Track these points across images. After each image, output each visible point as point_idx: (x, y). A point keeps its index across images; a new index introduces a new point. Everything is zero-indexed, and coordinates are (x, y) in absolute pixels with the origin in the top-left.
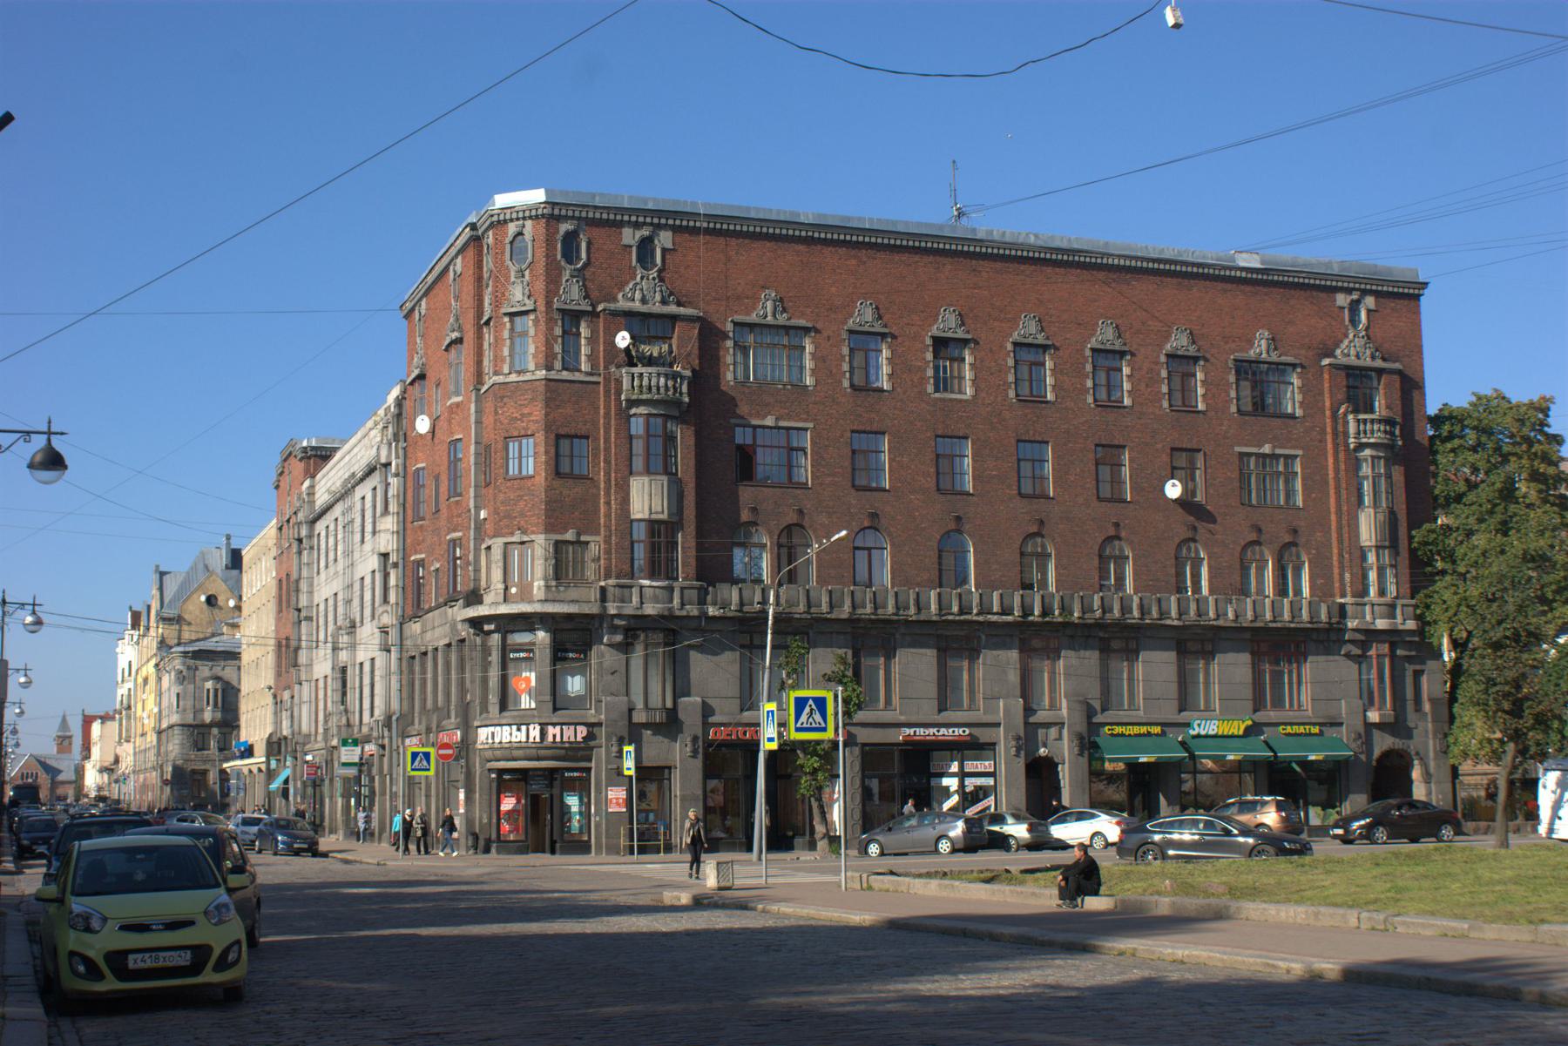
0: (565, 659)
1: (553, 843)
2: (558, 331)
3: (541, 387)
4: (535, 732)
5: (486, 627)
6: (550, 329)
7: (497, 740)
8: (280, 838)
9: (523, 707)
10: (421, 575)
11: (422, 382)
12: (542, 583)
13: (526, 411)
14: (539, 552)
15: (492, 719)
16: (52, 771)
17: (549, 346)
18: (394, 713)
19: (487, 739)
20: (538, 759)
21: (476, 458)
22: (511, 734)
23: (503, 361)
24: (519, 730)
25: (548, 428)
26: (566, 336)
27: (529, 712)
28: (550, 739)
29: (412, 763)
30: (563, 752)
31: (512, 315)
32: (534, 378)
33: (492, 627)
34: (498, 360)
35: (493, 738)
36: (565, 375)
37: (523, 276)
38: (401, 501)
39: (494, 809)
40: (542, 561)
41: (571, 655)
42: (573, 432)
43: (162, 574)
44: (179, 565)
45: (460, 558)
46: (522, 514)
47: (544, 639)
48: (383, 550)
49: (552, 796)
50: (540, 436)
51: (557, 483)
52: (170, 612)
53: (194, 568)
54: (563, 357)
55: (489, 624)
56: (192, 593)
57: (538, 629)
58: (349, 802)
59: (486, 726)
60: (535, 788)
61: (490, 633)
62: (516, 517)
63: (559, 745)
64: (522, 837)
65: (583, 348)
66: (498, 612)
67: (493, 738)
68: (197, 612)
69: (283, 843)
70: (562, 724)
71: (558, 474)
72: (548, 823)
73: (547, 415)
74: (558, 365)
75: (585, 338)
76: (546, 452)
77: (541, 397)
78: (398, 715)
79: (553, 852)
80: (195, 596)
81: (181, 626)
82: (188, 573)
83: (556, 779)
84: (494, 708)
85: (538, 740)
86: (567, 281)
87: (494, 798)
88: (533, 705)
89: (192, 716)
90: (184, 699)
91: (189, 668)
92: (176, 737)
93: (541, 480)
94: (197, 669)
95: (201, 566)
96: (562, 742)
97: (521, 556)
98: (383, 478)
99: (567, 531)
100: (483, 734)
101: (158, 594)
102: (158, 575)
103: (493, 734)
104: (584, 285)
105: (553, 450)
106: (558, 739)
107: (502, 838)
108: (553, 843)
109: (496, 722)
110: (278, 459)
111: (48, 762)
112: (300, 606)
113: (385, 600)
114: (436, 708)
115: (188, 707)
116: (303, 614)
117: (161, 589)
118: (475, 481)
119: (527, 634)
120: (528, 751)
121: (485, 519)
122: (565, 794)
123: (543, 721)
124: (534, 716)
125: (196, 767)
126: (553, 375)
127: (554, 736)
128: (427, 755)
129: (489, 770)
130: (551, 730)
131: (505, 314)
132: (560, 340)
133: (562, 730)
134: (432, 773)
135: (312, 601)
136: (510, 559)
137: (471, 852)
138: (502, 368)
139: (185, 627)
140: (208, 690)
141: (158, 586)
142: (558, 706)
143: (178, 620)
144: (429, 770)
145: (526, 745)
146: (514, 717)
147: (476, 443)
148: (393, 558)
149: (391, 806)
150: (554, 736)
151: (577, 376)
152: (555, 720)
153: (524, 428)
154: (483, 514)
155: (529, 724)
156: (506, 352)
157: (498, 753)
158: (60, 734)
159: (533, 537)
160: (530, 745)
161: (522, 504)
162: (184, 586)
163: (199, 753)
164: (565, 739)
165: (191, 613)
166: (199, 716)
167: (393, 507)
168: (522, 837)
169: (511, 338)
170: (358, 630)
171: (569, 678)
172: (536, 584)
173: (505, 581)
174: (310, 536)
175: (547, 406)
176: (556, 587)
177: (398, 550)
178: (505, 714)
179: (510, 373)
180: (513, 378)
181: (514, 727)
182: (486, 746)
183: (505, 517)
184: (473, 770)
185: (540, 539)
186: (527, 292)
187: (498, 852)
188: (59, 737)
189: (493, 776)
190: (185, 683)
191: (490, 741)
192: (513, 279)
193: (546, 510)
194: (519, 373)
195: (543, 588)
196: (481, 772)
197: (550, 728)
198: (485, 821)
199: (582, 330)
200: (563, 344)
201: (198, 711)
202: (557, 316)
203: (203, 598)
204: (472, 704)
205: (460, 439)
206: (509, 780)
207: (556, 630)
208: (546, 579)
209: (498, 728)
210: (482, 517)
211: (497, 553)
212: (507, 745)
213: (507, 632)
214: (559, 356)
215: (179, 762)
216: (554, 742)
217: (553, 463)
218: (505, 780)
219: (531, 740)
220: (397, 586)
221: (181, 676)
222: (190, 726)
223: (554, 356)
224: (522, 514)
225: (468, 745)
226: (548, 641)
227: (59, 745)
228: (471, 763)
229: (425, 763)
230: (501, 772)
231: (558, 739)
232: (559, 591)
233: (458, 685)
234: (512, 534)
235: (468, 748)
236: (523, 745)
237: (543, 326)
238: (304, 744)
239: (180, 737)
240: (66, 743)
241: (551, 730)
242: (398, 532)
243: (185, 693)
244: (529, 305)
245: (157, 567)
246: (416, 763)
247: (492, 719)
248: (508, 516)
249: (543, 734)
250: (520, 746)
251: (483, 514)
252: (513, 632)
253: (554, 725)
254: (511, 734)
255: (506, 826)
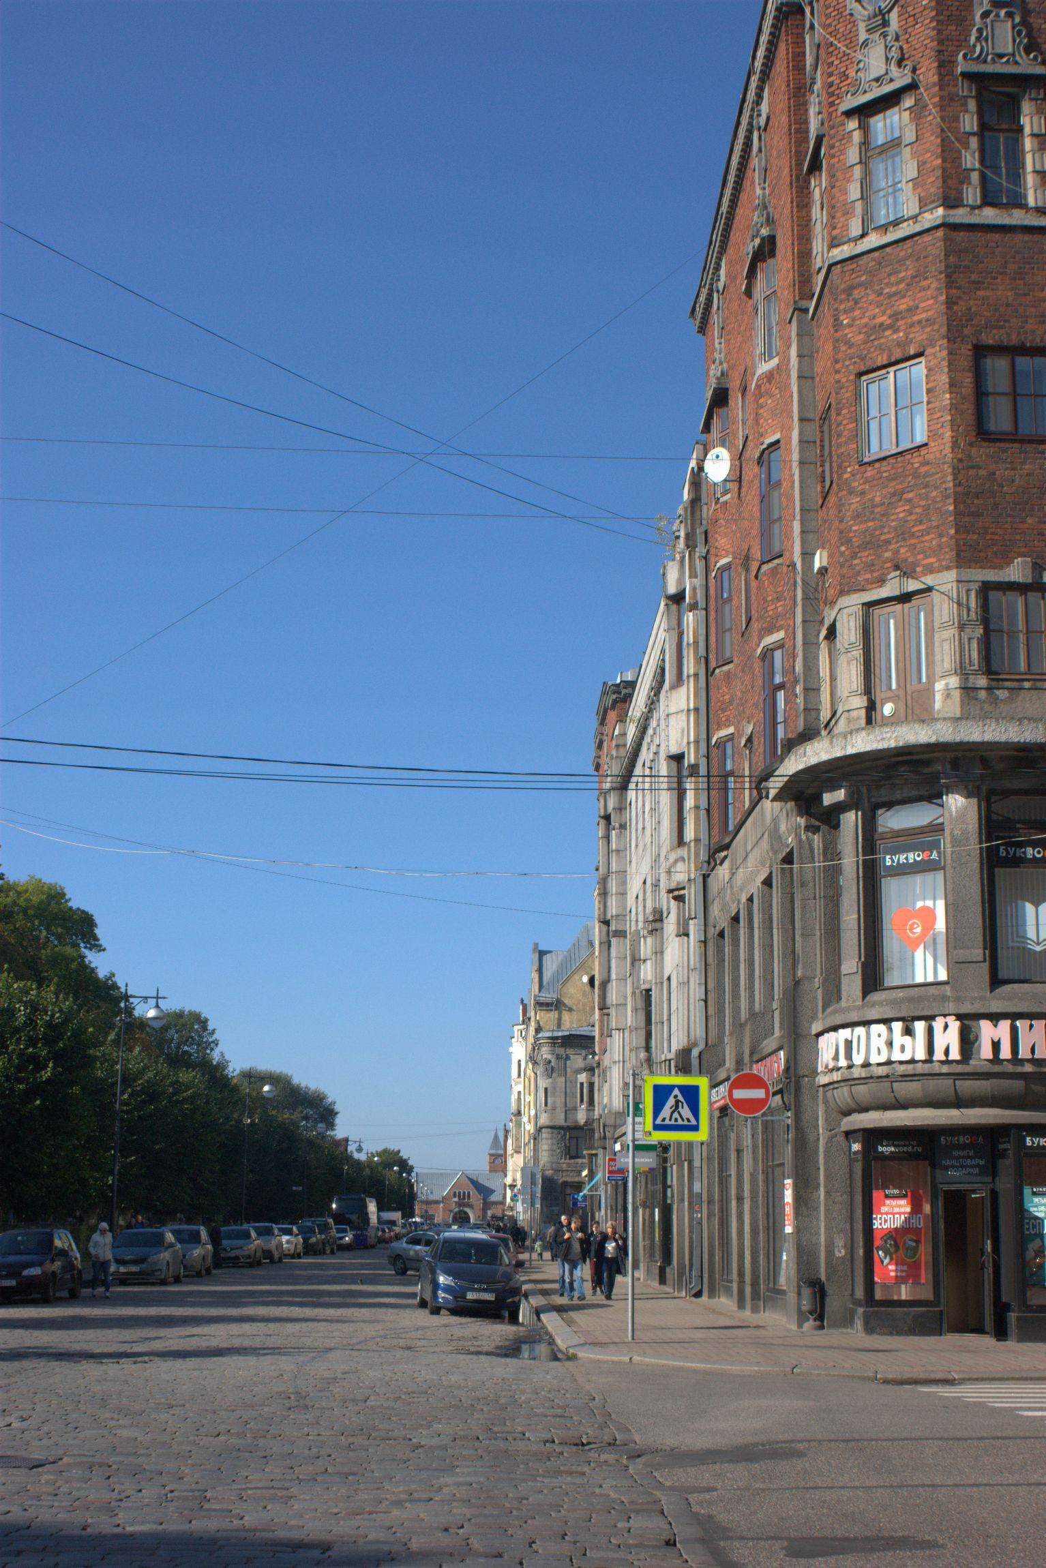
0: (1018, 862)
1: (1001, 1310)
2: (969, 122)
3: (935, 245)
4: (948, 1037)
5: (828, 799)
6: (949, 120)
7: (858, 1059)
8: (441, 1279)
9: (919, 979)
10: (729, 767)
11: (723, 411)
12: (954, 681)
13: (902, 305)
14: (943, 609)
15: (848, 1010)
16: (485, 1191)
17: (949, 153)
18: (695, 1045)
19: (836, 1058)
20: (959, 1102)
21: (801, 451)
22: (890, 1044)
23: (848, 213)
24: (908, 1032)
25: (953, 335)
26: (987, 134)
27: (932, 991)
28: (986, 1052)
29: (657, 1110)
30: (1019, 1085)
31: (865, 112)
32: (918, 228)
33: (840, 795)
34: (839, 211)
35: (849, 1056)
36: (990, 215)
37: (885, 23)
38: (702, 652)
39: (859, 1226)
40: (952, 632)
41: (1030, 852)
42: (1014, 340)
43: (542, 954)
44: (560, 943)
45: (781, 686)
46: (903, 534)
47: (961, 816)
48: (674, 750)
49: (994, 1195)
50: (939, 352)
51: (982, 452)
52: (547, 996)
53: (576, 945)
54: (983, 178)
55: (834, 788)
56: (574, 973)
57: (949, 790)
58: (652, 1215)
59: (835, 1029)
60: (955, 1176)
61: (840, 808)
62: (888, 542)
63: (1010, 1068)
64: (927, 1294)
65: (1029, 159)
66: (850, 751)
67: (849, 1056)
68: (579, 996)
69: (447, 1289)
70: (1014, 1016)
71: (982, 432)
72: (988, 1261)
73: (950, 303)
74: (972, 194)
75: (1033, 135)
76: (953, 385)
77: (936, 267)
78: (701, 1046)
79: (1001, 1333)
80: (576, 977)
81: (560, 1014)
82: (569, 950)
83: (1003, 1155)
84: (852, 985)
85: (955, 1055)
86: (985, 15)
87: (859, 1198)
88: (943, 975)
89: (562, 1116)
90: (553, 1094)
91: (558, 1057)
92: (544, 1141)
93: (943, 449)
94: (568, 1058)
95: (584, 943)
96: (1015, 1059)
97: (902, 628)
98: (674, 623)
99: (1009, 562)
100: (829, 1047)
101: (537, 976)
102: (537, 955)
103: (849, 1044)
104: (1024, 22)
105: (968, 380)
106: (1005, 1053)
107: (878, 1295)
108: (1001, 1310)
109: (854, 1017)
110: (595, 722)
111: (481, 1181)
112: (609, 917)
113: (681, 842)
114: (753, 1015)
115: (558, 1104)
116: (613, 927)
117: (540, 971)
118: (802, 500)
119: (924, 805)
120: (932, 1084)
121: (823, 571)
122: (1027, 1191)
123: (966, 1008)
124: (944, 998)
125: (569, 1179)
126: (960, 215)
127: (996, 1046)
128: (691, 1094)
129: (848, 1134)
130: (987, 1032)
131: (849, 114)
132: (974, 142)
133: (1014, 1031)
134: (702, 1135)
135: (625, 908)
136: (878, 643)
137: (809, 1324)
138: (846, 227)
139: (566, 1016)
140: (582, 1084)
141: (536, 968)
142: (1003, 974)
143: (556, 1005)
144: (695, 1128)
145: (926, 1068)
146: (895, 1003)
147: (801, 420)
148: (690, 758)
149: (691, 1219)
150: (996, 1046)
151: (1016, 217)
152: (996, 1007)
153: (899, 345)
154: (818, 561)
155: (932, 1018)
156: (854, 192)
157: (862, 1091)
158: (493, 1152)
159: (929, 580)
160: (936, 1068)
161: (901, 511)
162: (563, 966)
163: (572, 1161)
164: (1024, 1053)
165: (571, 997)
166: (570, 1116)
167: (690, 666)
168: (927, 1294)
169: (864, 162)
170: (665, 921)
171: (1029, 908)
172: (939, 686)
173: (868, 690)
174: (621, 809)
175: (950, 283)
176: (989, 689)
177: (697, 742)
178: (875, 997)
179: (863, 236)
180: (873, 240)
181: (897, 1026)
182: (836, 1076)
183: (864, 546)
184: (812, 1137)
185: (946, 580)
186: (894, 53)
187: (869, 1330)
188: (491, 1155)
189: (856, 1147)
190: (554, 1075)
191: (843, 1062)
192: (863, 36)
193: (958, 514)
194: (884, 228)
195: (957, 695)
196: (830, 1139)
197: (985, 1025)
198: (840, 1253)
199: (1025, 121)
200: (982, 150)
201: (569, 1110)
202: (964, 89)
203: (585, 979)
204: (805, 986)
205: (778, 442)
206: (892, 1157)
207: (991, 793)
208: (962, 670)
209: (860, 1030)
210: (817, 565)
211: (849, 632)
212: (882, 1071)
213: (877, 806)
214: (975, 177)
215: (549, 1173)
216: (996, 1059)
217: (969, 407)
218: (883, 1158)
219: (939, 1055)
220: (697, 807)
221: (549, 1067)
222: (561, 1128)
223: (963, 176)
224: (903, 534)
225: (799, 1078)
226: (972, 823)
227: (492, 1163)
228: (806, 1116)
229: (686, 1112)
230: (872, 1136)
231: (1005, 1053)
232: (995, 701)
233: (784, 955)
234: (882, 581)
235: (798, 1088)
236: (920, 1068)
237: (933, 116)
238: (615, 1127)
239: (550, 1141)
240: (498, 1161)
241: (987, 1032)
242: (696, 710)
243: (554, 1088)
244: (901, 79)
245: (536, 945)
246: (666, 1112)
247: (848, 1010)
248: (873, 543)
249: (968, 1041)
250: (911, 1072)
251: (818, 561)
252: (889, 805)
253: (995, 1018)
254: (890, 1044)
255: (888, 1268)
